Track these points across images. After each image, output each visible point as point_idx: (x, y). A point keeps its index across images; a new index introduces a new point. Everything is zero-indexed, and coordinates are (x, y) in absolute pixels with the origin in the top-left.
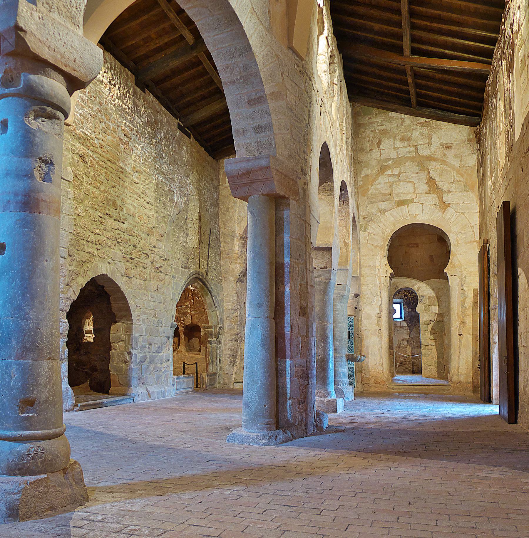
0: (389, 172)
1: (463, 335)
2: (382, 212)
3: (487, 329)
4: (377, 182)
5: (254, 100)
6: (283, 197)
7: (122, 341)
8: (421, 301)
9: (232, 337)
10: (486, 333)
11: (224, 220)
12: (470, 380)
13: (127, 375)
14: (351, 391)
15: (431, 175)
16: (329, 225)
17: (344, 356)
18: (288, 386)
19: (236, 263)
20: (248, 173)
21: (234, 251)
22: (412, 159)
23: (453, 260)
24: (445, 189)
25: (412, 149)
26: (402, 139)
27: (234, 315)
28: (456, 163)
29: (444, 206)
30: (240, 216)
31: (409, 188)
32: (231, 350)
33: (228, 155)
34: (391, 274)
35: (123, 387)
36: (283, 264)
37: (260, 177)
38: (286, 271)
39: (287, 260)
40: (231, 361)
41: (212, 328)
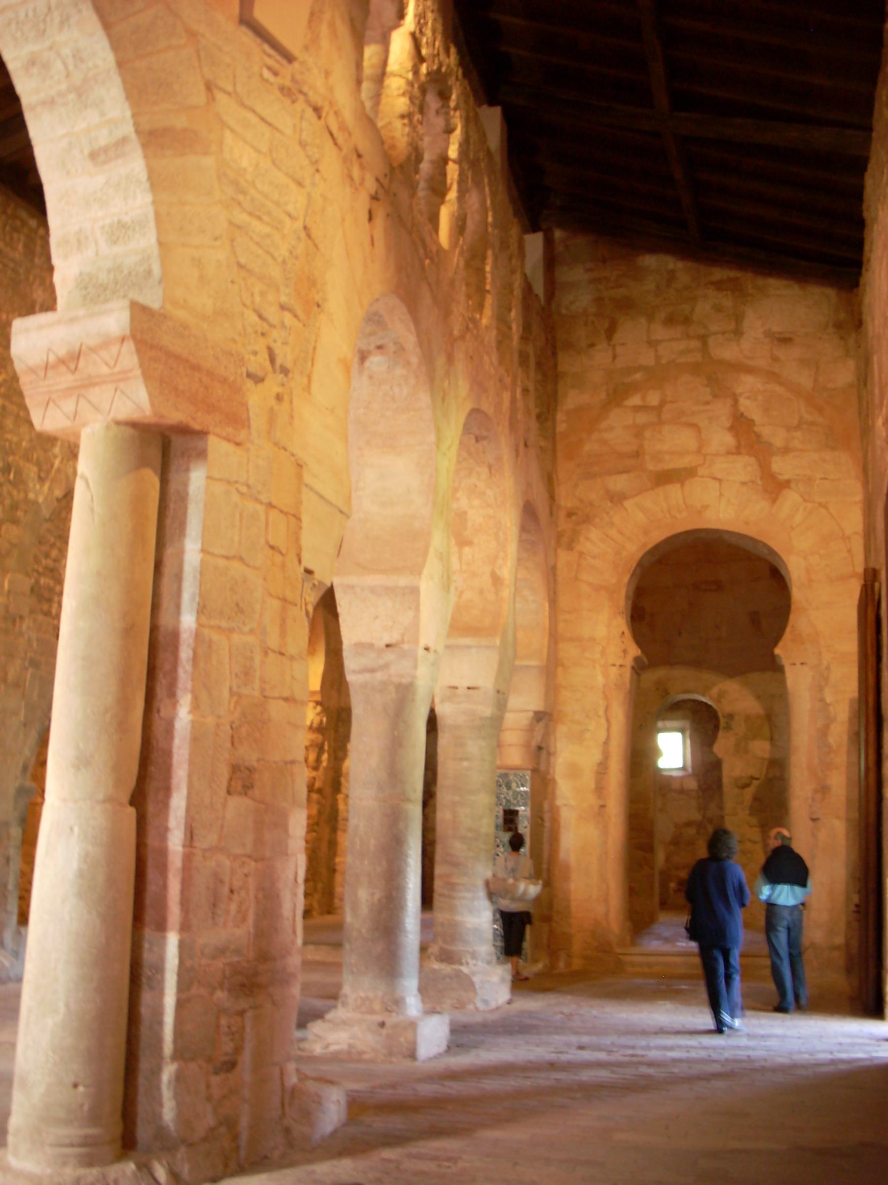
0: (635, 400)
2: (617, 498)
3: (872, 809)
4: (604, 425)
5: (105, 150)
6: (184, 431)
8: (728, 728)
10: (872, 819)
12: (839, 940)
14: (495, 979)
15: (742, 409)
17: (480, 883)
18: (169, 1019)
22: (695, 369)
23: (798, 622)
24: (778, 441)
25: (695, 344)
26: (670, 321)
28: (805, 380)
29: (774, 487)
31: (684, 439)
33: (30, 310)
34: (637, 659)
36: (175, 635)
37: (105, 370)
38: (185, 653)
39: (188, 621)
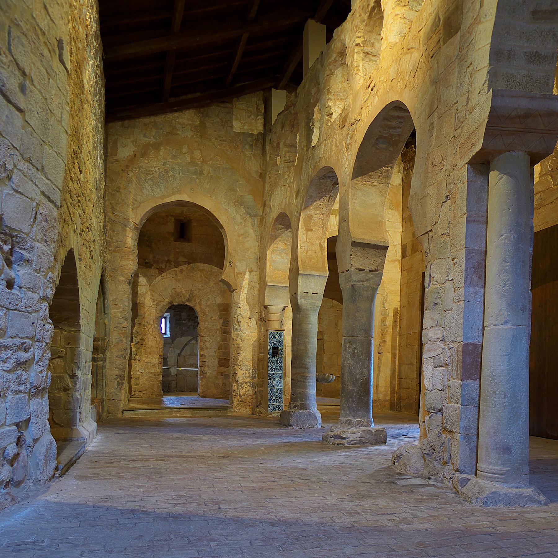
1: (384, 353)
7: (59, 357)
9: (120, 353)
11: (112, 202)
12: (388, 398)
13: (68, 409)
16: (379, 219)
19: (128, 259)
20: (527, 115)
21: (125, 243)
27: (123, 325)
30: (136, 200)
32: (120, 369)
35: (61, 429)
40: (119, 384)
41: (99, 341)
